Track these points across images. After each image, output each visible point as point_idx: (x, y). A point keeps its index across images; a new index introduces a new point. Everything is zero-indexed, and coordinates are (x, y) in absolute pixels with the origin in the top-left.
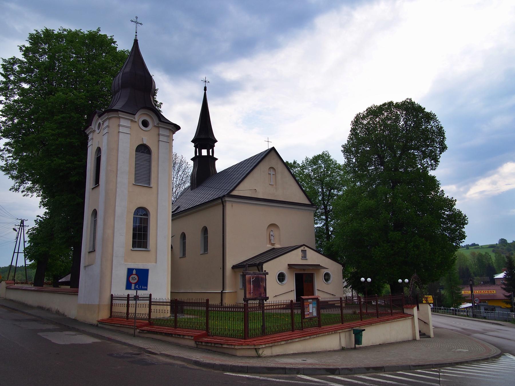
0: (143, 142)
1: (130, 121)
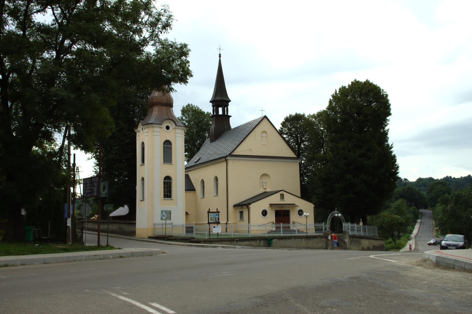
0: (167, 138)
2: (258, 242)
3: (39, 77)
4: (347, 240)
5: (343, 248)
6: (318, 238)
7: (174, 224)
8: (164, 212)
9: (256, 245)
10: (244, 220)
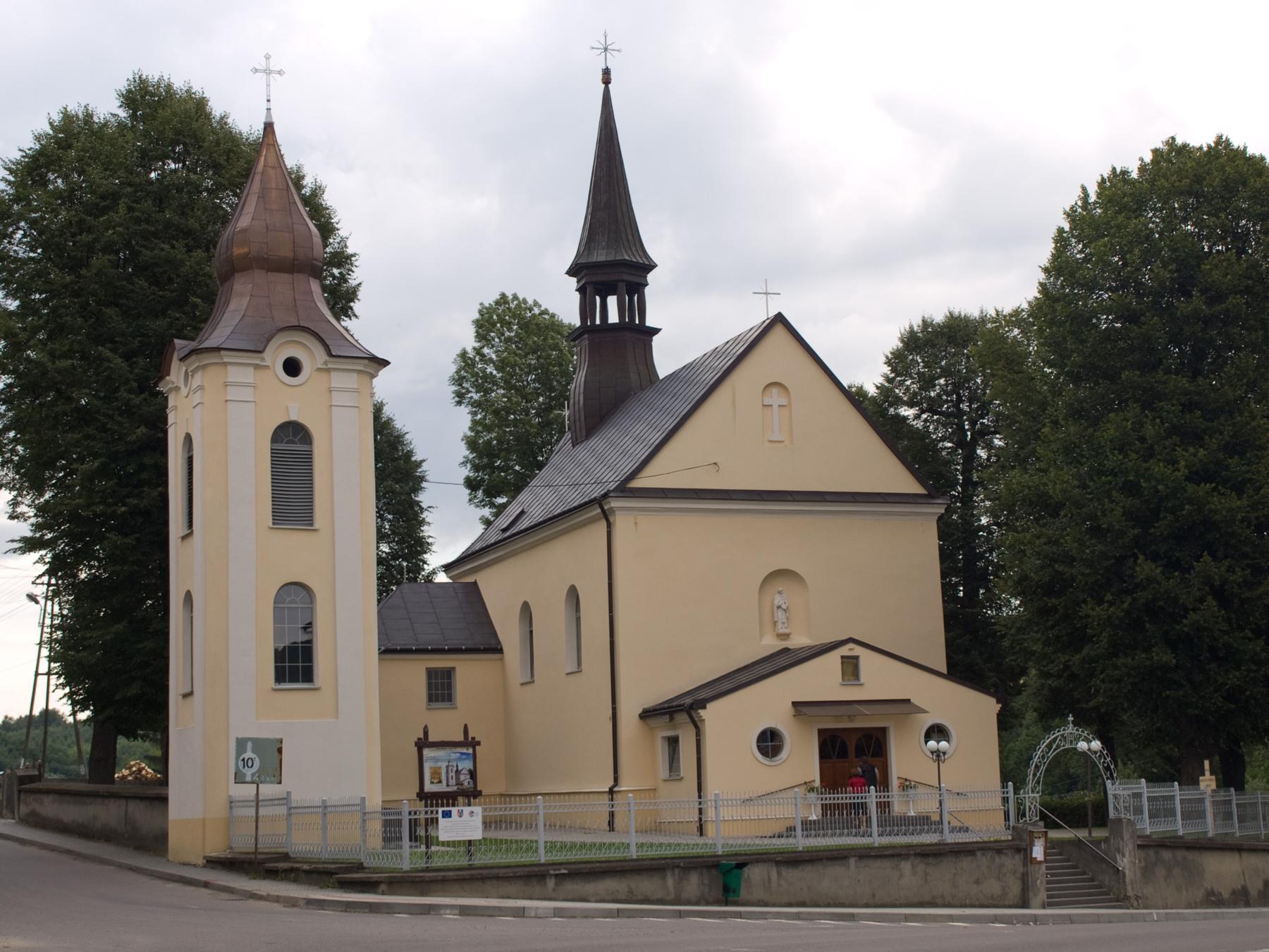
0: (289, 415)
1: (251, 369)
2: (670, 881)
3: (9, 233)
4: (1125, 860)
5: (1112, 896)
6: (979, 854)
7: (296, 798)
8: (249, 745)
9: (659, 895)
10: (682, 775)
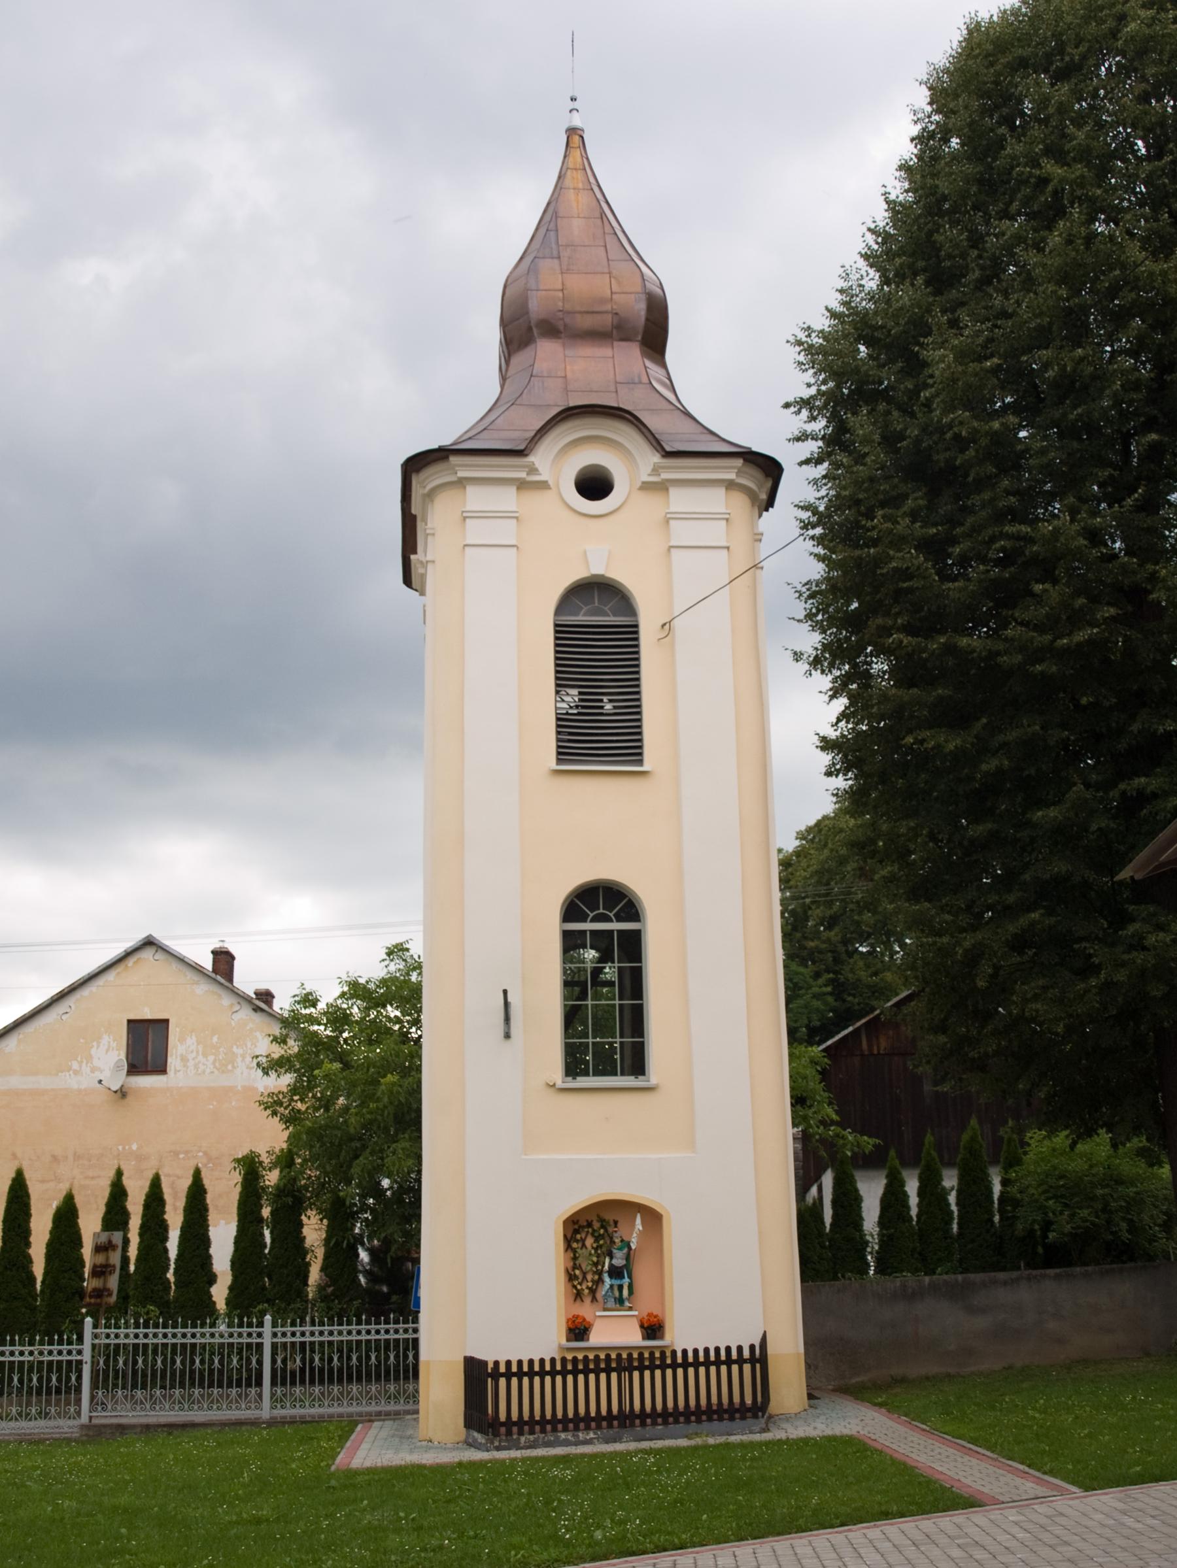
1: (512, 491)
